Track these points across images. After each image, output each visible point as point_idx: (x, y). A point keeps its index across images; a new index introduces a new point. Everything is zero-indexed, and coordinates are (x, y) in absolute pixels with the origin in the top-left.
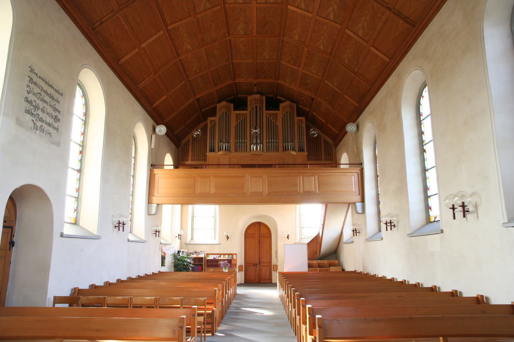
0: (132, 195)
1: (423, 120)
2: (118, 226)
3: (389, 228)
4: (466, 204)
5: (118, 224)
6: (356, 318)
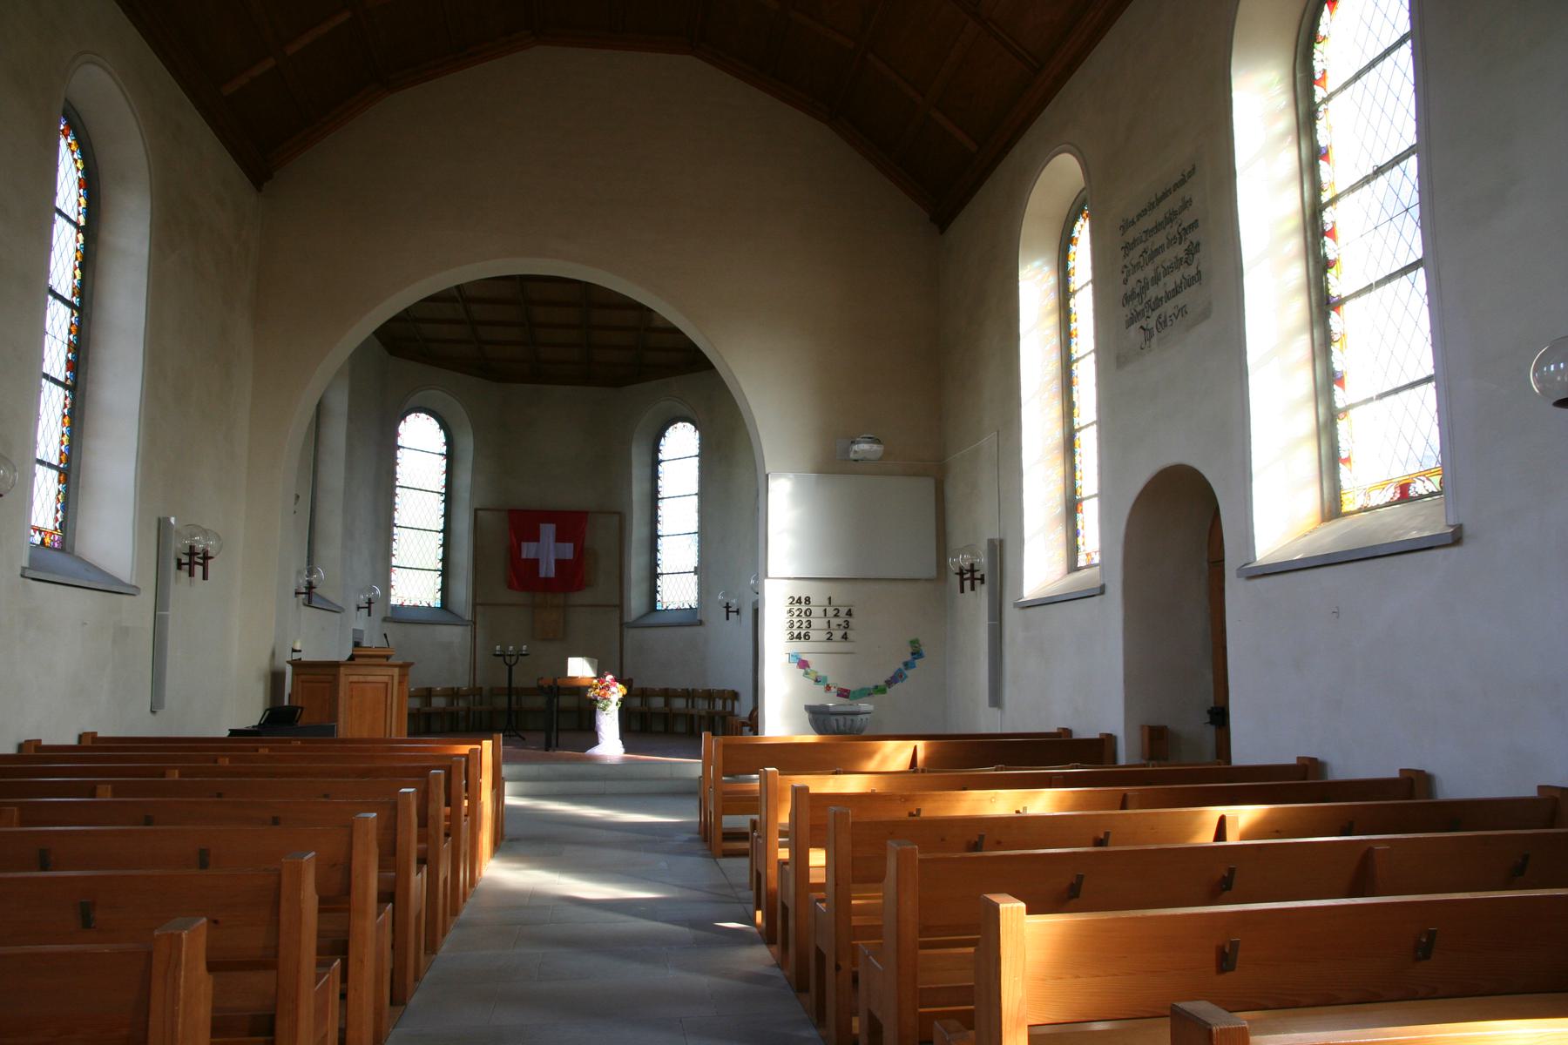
1: (1326, 100)
3: (967, 584)
4: (976, 568)
6: (63, 131)
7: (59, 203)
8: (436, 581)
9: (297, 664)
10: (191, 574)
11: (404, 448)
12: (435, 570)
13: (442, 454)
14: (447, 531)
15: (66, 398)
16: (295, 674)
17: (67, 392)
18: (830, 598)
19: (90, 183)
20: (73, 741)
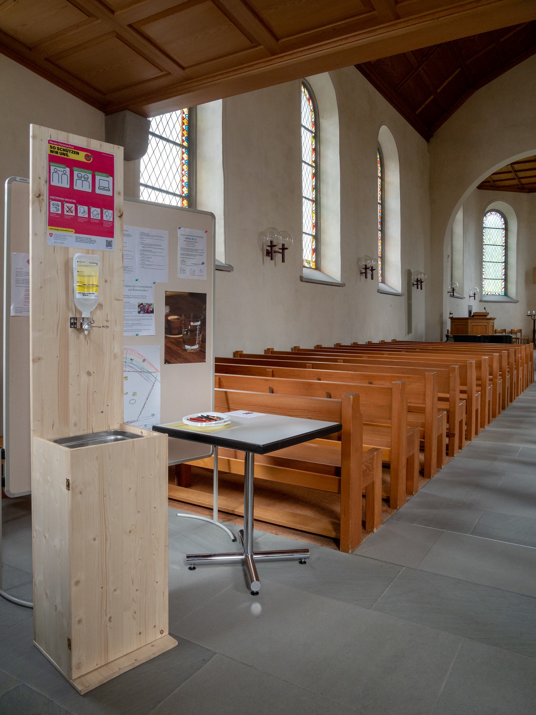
0: (381, 231)
2: (365, 272)
5: (416, 282)
7: (304, 123)
8: (501, 284)
9: (452, 319)
10: (366, 277)
11: (486, 228)
12: (501, 279)
13: (503, 229)
14: (506, 262)
15: (183, 153)
16: (452, 322)
17: (184, 150)
18: (68, 481)
19: (316, 111)
20: (391, 341)
